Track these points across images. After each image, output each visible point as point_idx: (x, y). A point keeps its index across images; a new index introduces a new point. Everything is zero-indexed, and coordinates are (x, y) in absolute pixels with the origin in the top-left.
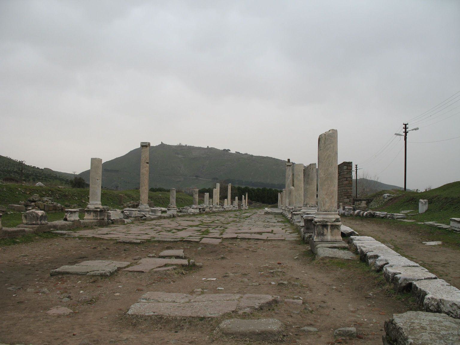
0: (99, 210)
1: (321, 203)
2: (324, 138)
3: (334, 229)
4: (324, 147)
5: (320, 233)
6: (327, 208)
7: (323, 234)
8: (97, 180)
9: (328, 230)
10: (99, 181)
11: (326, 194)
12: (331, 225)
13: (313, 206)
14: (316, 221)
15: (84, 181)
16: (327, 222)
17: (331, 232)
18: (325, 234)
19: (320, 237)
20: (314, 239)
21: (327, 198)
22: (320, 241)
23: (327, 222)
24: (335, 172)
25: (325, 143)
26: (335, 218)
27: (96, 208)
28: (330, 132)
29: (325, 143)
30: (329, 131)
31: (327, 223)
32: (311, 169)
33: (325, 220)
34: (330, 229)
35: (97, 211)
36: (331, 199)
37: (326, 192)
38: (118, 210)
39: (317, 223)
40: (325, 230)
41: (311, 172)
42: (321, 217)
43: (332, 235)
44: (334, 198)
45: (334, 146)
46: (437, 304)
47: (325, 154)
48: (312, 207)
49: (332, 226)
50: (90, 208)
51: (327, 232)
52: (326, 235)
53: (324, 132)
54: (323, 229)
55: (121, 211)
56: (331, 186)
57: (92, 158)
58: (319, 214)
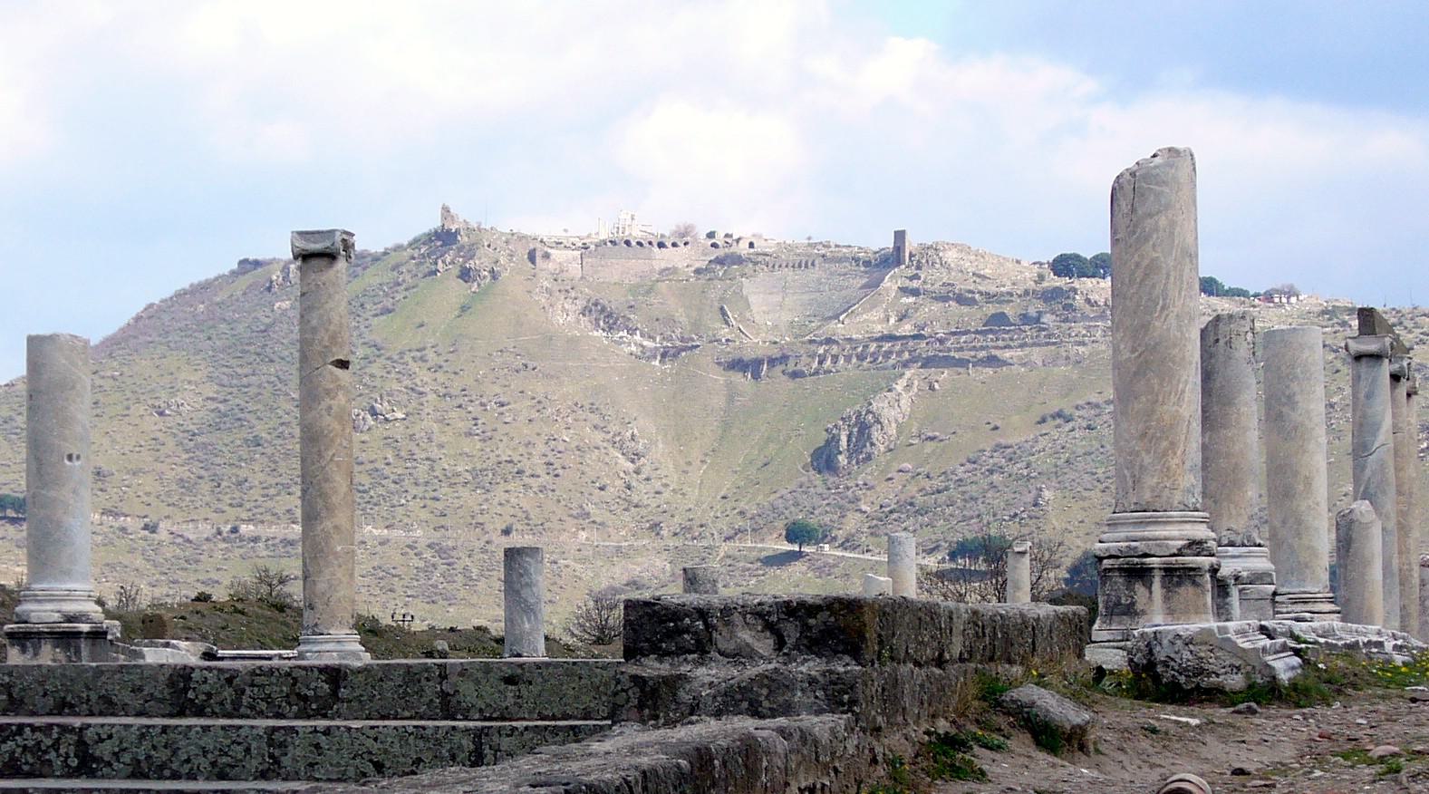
0: (85, 627)
1: (1125, 476)
2: (1128, 188)
3: (1179, 584)
4: (1131, 228)
5: (1118, 604)
6: (1147, 496)
7: (1130, 611)
8: (70, 457)
9: (1151, 593)
10: (77, 463)
11: (1144, 435)
12: (1166, 570)
13: (1238, 540)
14: (1098, 553)
15: (151, 306)
16: (1146, 555)
17: (1167, 599)
18: (1139, 607)
19: (1120, 623)
20: (1094, 633)
21: (1148, 452)
22: (1120, 638)
23: (1146, 555)
24: (1179, 334)
25: (1133, 210)
26: (1182, 539)
27: (71, 619)
28: (1157, 160)
29: (1133, 210)
30: (1154, 156)
31: (1144, 560)
32: (1222, 342)
33: (1136, 548)
34: (1163, 587)
35: (77, 635)
36: (1165, 454)
37: (1141, 426)
38: (183, 644)
39: (1105, 561)
40: (1140, 589)
41: (1221, 359)
42: (1123, 535)
43: (1170, 612)
44: (1179, 453)
45: (1172, 224)
46: (1148, 645)
47: (1136, 258)
48: (1232, 544)
49: (1169, 572)
50: (34, 617)
51: (1150, 598)
52: (1144, 612)
53: (1131, 164)
54: (1130, 587)
55: (203, 649)
56: (1161, 399)
57: (34, 333)
58: (1115, 524)
